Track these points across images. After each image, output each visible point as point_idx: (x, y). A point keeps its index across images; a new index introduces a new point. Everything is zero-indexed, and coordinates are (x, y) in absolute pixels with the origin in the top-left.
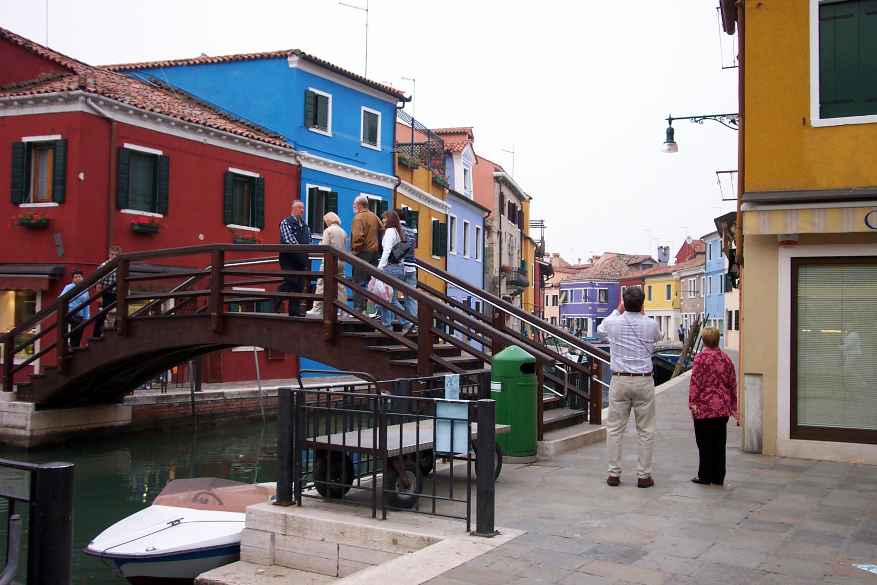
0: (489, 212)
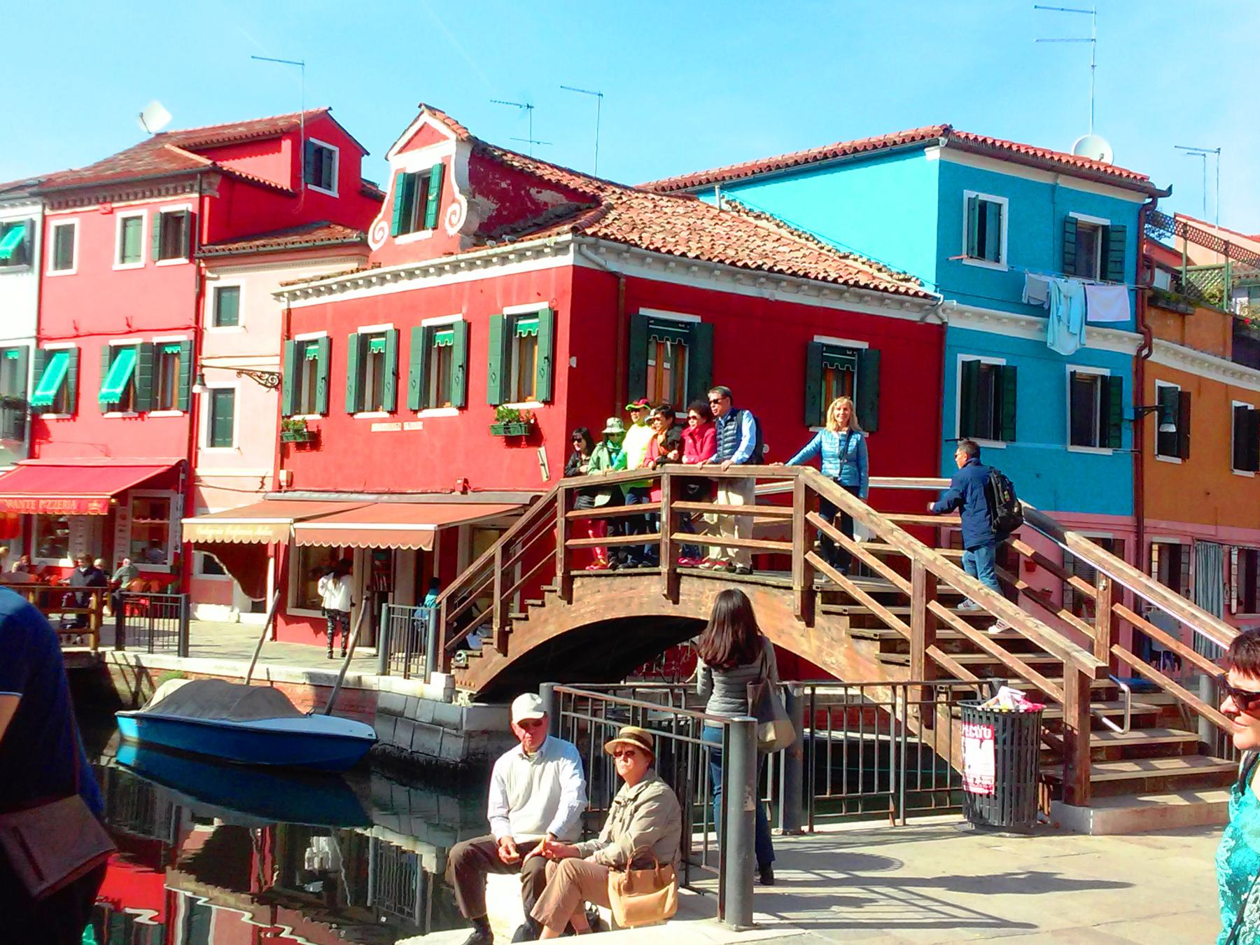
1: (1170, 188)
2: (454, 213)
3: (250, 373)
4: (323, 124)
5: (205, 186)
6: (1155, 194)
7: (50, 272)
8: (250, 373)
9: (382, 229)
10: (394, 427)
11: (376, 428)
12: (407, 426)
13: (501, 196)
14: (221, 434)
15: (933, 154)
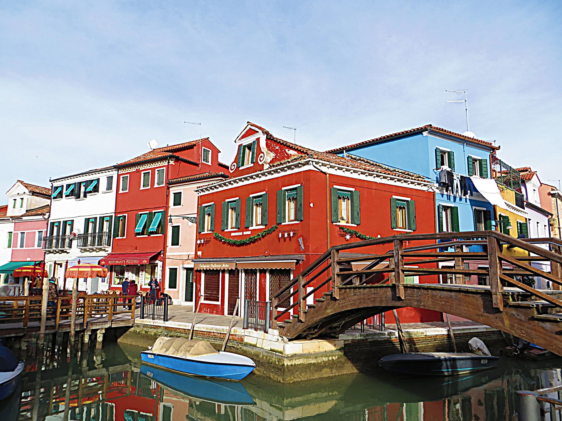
0: (552, 215)
1: (499, 147)
2: (261, 157)
3: (187, 218)
4: (206, 142)
5: (170, 161)
6: (494, 149)
7: (121, 192)
8: (187, 218)
9: (234, 165)
10: (241, 234)
11: (233, 234)
12: (245, 233)
13: (276, 152)
14: (175, 242)
15: (425, 133)
